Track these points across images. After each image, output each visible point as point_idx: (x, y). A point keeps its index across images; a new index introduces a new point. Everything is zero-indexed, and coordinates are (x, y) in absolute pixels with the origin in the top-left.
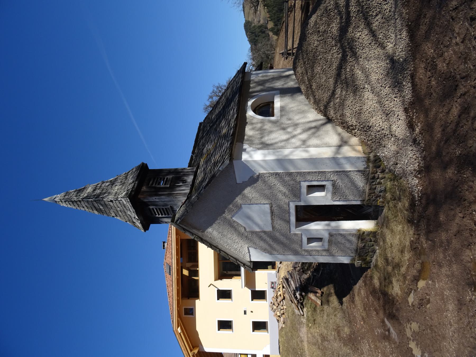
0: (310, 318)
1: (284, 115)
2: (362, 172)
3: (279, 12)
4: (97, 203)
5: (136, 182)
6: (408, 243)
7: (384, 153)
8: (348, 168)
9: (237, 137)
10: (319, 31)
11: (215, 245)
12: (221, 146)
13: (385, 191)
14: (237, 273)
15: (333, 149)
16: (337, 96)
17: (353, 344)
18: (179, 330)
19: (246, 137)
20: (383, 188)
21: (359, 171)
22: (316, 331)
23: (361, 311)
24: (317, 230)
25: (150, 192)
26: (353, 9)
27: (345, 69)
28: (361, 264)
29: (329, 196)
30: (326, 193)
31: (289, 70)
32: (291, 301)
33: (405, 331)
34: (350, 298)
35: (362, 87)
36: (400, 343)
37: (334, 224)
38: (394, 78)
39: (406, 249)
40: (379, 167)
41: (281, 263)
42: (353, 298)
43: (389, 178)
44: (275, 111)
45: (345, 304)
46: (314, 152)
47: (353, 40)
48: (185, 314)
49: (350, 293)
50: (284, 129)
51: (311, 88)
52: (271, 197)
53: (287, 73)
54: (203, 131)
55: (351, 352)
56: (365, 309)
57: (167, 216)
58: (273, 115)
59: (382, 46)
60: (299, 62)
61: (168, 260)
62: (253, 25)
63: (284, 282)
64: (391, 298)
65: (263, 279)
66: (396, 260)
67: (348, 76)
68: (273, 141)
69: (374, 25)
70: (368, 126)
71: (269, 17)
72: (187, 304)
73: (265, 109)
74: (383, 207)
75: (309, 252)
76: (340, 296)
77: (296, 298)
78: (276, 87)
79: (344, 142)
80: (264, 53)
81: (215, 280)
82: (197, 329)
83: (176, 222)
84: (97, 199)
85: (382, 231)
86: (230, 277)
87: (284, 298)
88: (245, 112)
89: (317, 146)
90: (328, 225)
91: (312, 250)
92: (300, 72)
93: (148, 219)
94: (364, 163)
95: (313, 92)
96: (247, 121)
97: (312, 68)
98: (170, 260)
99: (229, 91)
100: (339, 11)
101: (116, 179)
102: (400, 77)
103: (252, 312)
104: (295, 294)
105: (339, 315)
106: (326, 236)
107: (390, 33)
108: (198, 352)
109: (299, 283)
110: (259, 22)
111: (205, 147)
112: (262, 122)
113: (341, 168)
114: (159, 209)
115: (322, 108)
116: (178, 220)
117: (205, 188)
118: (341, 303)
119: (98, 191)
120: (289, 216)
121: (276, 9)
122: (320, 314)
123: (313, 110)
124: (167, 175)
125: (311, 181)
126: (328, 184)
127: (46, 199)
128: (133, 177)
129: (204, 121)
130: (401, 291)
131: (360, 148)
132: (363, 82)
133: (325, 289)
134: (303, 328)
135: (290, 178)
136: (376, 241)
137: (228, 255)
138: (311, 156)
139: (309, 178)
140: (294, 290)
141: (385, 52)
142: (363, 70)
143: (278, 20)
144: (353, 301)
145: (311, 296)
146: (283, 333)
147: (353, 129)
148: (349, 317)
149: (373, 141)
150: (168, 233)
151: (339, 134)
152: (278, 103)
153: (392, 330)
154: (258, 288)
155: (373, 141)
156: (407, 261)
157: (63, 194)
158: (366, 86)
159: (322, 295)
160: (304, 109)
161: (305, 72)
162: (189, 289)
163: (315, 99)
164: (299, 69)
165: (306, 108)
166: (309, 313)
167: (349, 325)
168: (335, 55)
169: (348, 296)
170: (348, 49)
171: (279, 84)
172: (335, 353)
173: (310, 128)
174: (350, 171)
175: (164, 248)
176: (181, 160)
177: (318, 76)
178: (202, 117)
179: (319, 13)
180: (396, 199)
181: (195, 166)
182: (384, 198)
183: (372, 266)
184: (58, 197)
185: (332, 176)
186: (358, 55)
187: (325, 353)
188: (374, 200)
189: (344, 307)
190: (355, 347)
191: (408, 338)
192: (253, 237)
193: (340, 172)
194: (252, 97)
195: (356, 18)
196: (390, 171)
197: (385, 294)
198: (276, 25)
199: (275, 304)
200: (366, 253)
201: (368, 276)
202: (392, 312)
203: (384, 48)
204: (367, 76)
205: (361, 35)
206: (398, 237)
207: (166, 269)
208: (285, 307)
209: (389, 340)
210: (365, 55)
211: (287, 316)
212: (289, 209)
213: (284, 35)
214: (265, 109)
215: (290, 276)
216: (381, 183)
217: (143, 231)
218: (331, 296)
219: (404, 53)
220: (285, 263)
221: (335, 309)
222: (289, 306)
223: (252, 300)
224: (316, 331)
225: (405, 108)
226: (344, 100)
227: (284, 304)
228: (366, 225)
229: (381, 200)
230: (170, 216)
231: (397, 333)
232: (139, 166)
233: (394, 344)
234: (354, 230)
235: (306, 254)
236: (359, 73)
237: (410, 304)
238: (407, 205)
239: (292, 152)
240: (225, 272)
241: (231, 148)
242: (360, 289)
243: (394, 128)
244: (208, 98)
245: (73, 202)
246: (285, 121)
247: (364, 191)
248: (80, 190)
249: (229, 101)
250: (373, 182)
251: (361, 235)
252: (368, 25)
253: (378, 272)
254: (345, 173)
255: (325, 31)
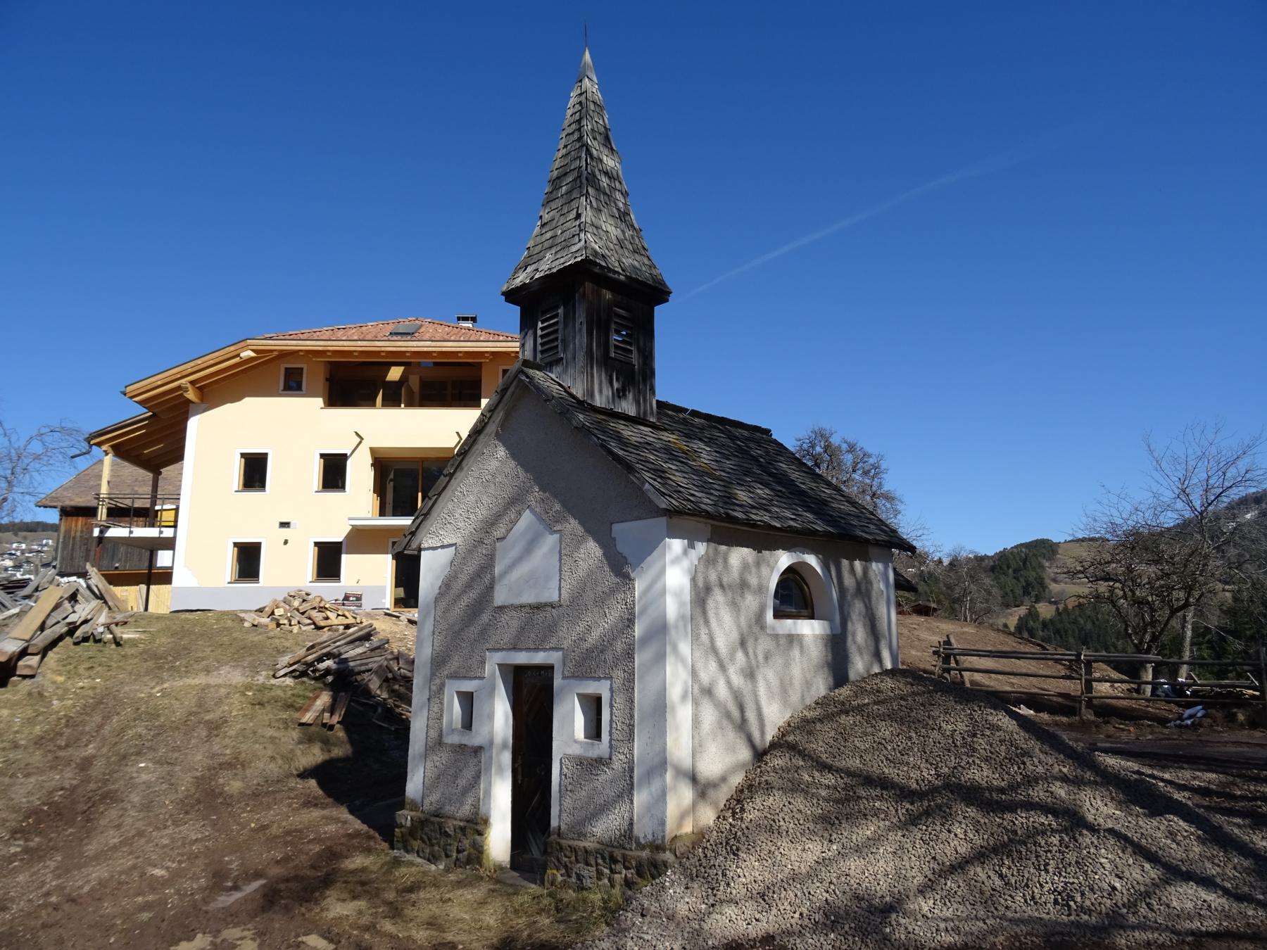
0: (268, 695)
1: (778, 645)
2: (628, 833)
3: (1067, 635)
4: (575, 180)
5: (622, 278)
6: (450, 937)
7: (672, 885)
8: (640, 798)
9: (726, 528)
10: (974, 735)
11: (464, 463)
12: (705, 488)
13: (581, 888)
14: (389, 507)
15: (687, 763)
16: (817, 774)
17: (199, 802)
18: (248, 354)
19: (724, 548)
20: (587, 882)
21: (631, 824)
22: (234, 707)
23: (284, 824)
24: (491, 717)
25: (600, 309)
26: (1022, 820)
27: (881, 798)
28: (401, 826)
29: (576, 750)
30: (580, 743)
31: (894, 658)
32: (313, 647)
33: (236, 925)
34: (315, 798)
35: (835, 836)
36: (206, 912)
37: (507, 758)
38: (847, 913)
39: (435, 933)
40: (640, 874)
41: (411, 622)
42: (316, 805)
43: (610, 896)
44: (789, 622)
45: (300, 785)
46: (682, 715)
47: (946, 816)
48: (287, 369)
49: (330, 796)
50: (743, 643)
51: (842, 712)
52: (576, 605)
53: (886, 655)
54: (749, 439)
55: (180, 796)
56: (288, 833)
57: (539, 348)
58: (778, 615)
59: (927, 886)
60: (907, 684)
61: (428, 330)
62: (1047, 564)
63: (361, 629)
64: (317, 894)
65: (370, 574)
66: (409, 911)
67: (863, 804)
68: (711, 614)
69: (979, 869)
70: (738, 850)
71: (1066, 609)
72: (315, 375)
73: (794, 596)
74: (542, 883)
75: (437, 694)
76: (323, 774)
77: (320, 660)
78: (849, 624)
79: (702, 789)
80: (966, 592)
81: (372, 450)
82: (247, 400)
83: (522, 372)
84: (584, 181)
85: (482, 878)
86: (380, 488)
87: (319, 628)
88: (788, 547)
89: (696, 723)
90: (504, 746)
91: (442, 703)
92: (882, 686)
93: (532, 301)
94: (650, 837)
95: (829, 717)
96: (766, 553)
97: (891, 717)
98: (427, 336)
99: (846, 507)
100: (1019, 785)
101: (632, 226)
102: (847, 927)
103: (286, 542)
104: (329, 656)
105: (274, 769)
106: (476, 738)
107: (955, 906)
108: (189, 401)
109: (357, 669)
110: (1055, 580)
111: (706, 444)
112: (761, 589)
113: (640, 780)
114: (556, 331)
115: (790, 738)
116: (527, 377)
117: (602, 446)
118: (304, 775)
119: (604, 181)
120: (528, 649)
121: (1089, 626)
122: (278, 720)
123: (787, 716)
124: (639, 349)
125: (611, 706)
126: (602, 747)
127: (587, 56)
128: (634, 267)
129: (775, 442)
130: (335, 919)
131: (688, 828)
132: (844, 840)
133: (341, 733)
134: (243, 675)
135: (618, 655)
136: (457, 863)
137: (439, 494)
138: (673, 709)
139: (620, 700)
140: (340, 654)
141: (911, 894)
142: (875, 840)
143: (1058, 632)
144: (310, 803)
145: (325, 699)
146: (230, 623)
147: (734, 813)
148: (268, 793)
149: (704, 861)
150: (500, 336)
151: (724, 779)
152: (811, 629)
153: (237, 895)
154: (349, 563)
155: (704, 859)
156: (406, 934)
157: (599, 97)
158: (835, 847)
159: (324, 725)
160: (791, 692)
161: (882, 697)
162: (351, 383)
163: (813, 721)
164: (889, 683)
165: (795, 697)
166: (279, 692)
167: (248, 792)
168: (914, 774)
169: (321, 792)
170: (925, 805)
171: (858, 633)
172: (176, 755)
173: (742, 709)
174: (632, 802)
175: (459, 319)
176: (672, 386)
177: (869, 730)
178: (789, 435)
179: (1020, 736)
180: (560, 910)
181: (658, 419)
182: (565, 885)
183: (396, 853)
184: (591, 86)
185: (622, 757)
186: (911, 828)
187: (178, 728)
188: (558, 860)
189: (292, 783)
190: (192, 807)
191: (219, 931)
192: (476, 576)
193: (631, 777)
194: (826, 567)
195: (999, 825)
196: (628, 900)
197: (327, 882)
198: (1045, 625)
199: (305, 605)
200: (430, 840)
201: (372, 843)
202: (282, 898)
203: (921, 892)
204: (858, 850)
205: (958, 837)
206: (466, 917)
207: (405, 324)
208: (295, 629)
209: (212, 889)
210: (909, 846)
211: (272, 634)
212: (545, 650)
213: (1008, 649)
214: (794, 596)
215: (376, 645)
216: (599, 879)
217: (504, 289)
218: (322, 749)
219: (903, 937)
220: (411, 632)
221: (288, 759)
222: (299, 641)
223: (316, 544)
224: (234, 707)
225: (773, 937)
226: (807, 793)
227: (304, 628)
228: (499, 840)
229: (560, 878)
230: (539, 356)
231: (230, 906)
232: (662, 283)
233: (203, 899)
234: (489, 810)
235: (434, 688)
236: (869, 829)
237: (304, 939)
238: (543, 936)
239: (683, 661)
240: (392, 476)
241: (698, 513)
242: (338, 821)
243: (730, 911)
244: (851, 439)
245: (579, 121)
246: (764, 644)
247: (582, 835)
248: (607, 138)
249: (819, 507)
250: (604, 858)
251: (477, 824)
252: (980, 856)
253: (381, 867)
254: (628, 791)
255: (974, 750)
